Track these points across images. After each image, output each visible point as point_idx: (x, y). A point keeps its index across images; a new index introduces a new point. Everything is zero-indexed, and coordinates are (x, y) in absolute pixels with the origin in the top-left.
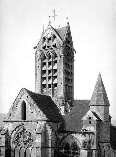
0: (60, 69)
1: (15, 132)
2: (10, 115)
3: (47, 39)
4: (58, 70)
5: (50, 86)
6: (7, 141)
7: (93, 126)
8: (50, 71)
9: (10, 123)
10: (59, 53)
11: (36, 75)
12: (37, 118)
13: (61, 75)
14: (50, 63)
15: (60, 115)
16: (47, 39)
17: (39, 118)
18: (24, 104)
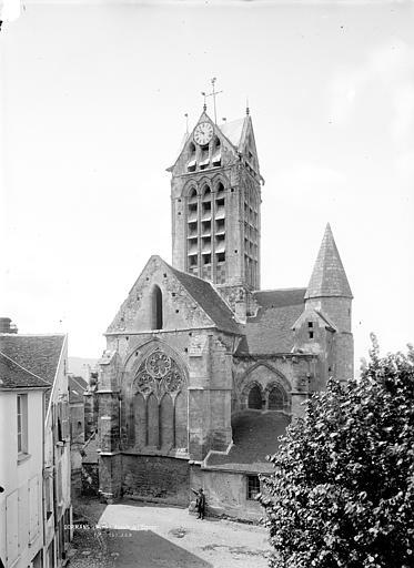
0: (232, 218)
1: (134, 358)
2: (122, 319)
3: (198, 149)
4: (227, 223)
5: (207, 258)
6: (115, 380)
7: (318, 341)
8: (207, 225)
9: (123, 341)
10: (218, 186)
11: (174, 234)
12: (184, 317)
13: (234, 233)
14: (207, 206)
15: (235, 324)
16: (198, 149)
17: (196, 325)
18: (158, 294)
